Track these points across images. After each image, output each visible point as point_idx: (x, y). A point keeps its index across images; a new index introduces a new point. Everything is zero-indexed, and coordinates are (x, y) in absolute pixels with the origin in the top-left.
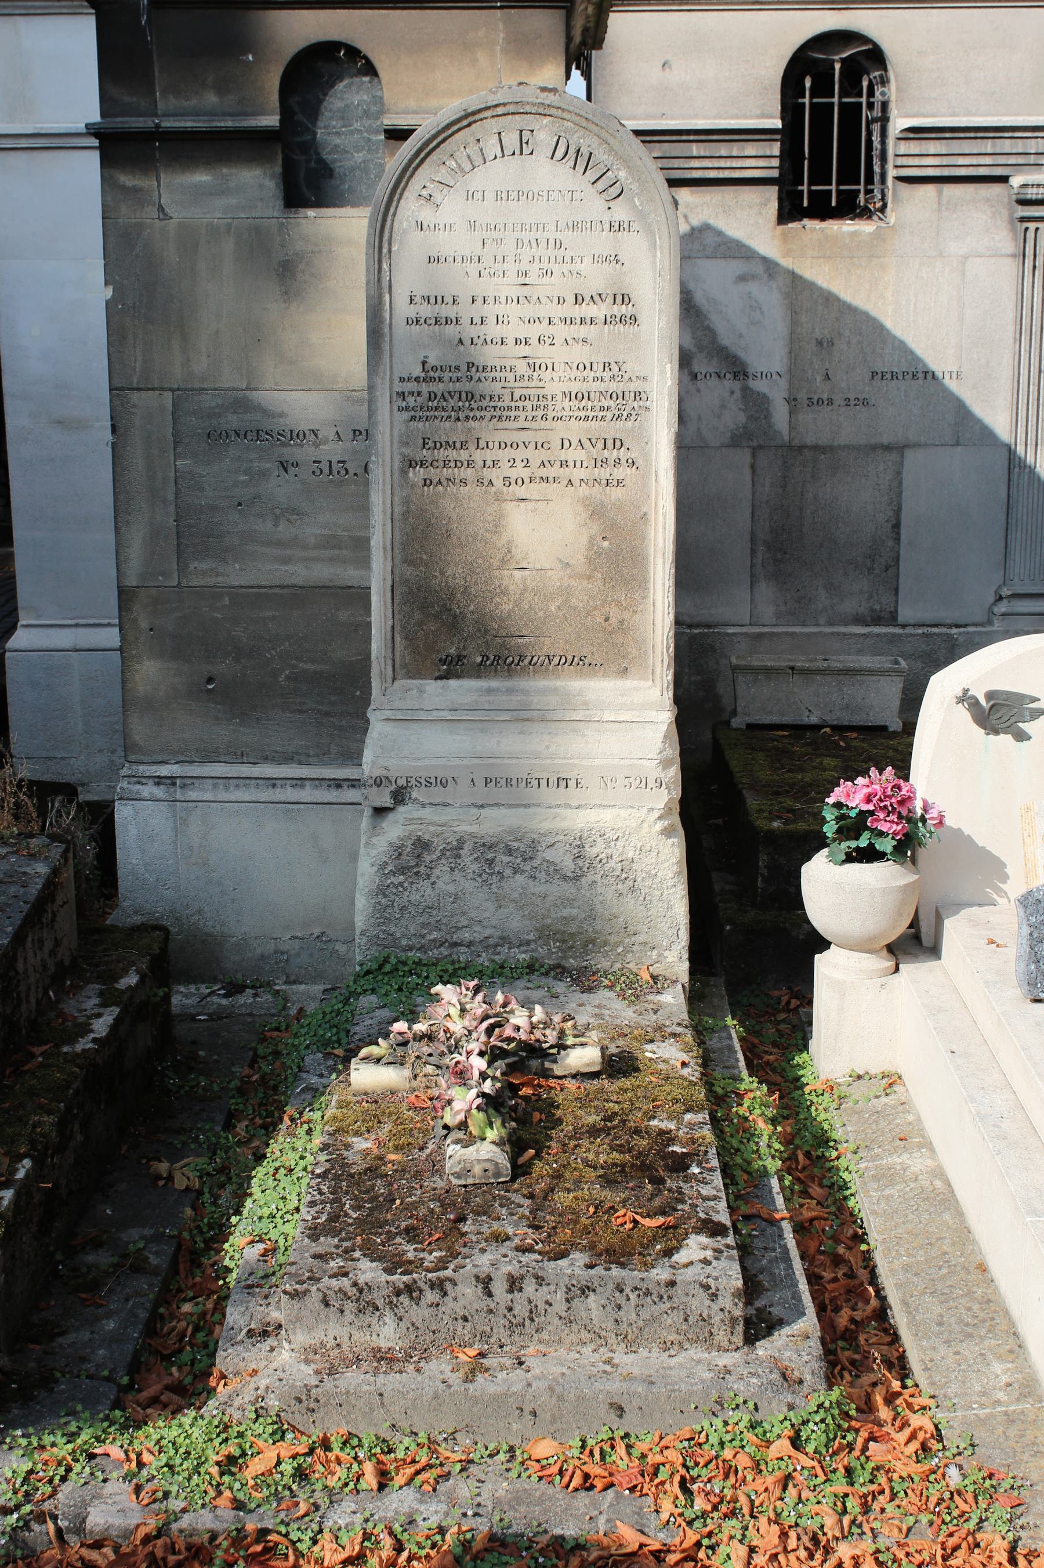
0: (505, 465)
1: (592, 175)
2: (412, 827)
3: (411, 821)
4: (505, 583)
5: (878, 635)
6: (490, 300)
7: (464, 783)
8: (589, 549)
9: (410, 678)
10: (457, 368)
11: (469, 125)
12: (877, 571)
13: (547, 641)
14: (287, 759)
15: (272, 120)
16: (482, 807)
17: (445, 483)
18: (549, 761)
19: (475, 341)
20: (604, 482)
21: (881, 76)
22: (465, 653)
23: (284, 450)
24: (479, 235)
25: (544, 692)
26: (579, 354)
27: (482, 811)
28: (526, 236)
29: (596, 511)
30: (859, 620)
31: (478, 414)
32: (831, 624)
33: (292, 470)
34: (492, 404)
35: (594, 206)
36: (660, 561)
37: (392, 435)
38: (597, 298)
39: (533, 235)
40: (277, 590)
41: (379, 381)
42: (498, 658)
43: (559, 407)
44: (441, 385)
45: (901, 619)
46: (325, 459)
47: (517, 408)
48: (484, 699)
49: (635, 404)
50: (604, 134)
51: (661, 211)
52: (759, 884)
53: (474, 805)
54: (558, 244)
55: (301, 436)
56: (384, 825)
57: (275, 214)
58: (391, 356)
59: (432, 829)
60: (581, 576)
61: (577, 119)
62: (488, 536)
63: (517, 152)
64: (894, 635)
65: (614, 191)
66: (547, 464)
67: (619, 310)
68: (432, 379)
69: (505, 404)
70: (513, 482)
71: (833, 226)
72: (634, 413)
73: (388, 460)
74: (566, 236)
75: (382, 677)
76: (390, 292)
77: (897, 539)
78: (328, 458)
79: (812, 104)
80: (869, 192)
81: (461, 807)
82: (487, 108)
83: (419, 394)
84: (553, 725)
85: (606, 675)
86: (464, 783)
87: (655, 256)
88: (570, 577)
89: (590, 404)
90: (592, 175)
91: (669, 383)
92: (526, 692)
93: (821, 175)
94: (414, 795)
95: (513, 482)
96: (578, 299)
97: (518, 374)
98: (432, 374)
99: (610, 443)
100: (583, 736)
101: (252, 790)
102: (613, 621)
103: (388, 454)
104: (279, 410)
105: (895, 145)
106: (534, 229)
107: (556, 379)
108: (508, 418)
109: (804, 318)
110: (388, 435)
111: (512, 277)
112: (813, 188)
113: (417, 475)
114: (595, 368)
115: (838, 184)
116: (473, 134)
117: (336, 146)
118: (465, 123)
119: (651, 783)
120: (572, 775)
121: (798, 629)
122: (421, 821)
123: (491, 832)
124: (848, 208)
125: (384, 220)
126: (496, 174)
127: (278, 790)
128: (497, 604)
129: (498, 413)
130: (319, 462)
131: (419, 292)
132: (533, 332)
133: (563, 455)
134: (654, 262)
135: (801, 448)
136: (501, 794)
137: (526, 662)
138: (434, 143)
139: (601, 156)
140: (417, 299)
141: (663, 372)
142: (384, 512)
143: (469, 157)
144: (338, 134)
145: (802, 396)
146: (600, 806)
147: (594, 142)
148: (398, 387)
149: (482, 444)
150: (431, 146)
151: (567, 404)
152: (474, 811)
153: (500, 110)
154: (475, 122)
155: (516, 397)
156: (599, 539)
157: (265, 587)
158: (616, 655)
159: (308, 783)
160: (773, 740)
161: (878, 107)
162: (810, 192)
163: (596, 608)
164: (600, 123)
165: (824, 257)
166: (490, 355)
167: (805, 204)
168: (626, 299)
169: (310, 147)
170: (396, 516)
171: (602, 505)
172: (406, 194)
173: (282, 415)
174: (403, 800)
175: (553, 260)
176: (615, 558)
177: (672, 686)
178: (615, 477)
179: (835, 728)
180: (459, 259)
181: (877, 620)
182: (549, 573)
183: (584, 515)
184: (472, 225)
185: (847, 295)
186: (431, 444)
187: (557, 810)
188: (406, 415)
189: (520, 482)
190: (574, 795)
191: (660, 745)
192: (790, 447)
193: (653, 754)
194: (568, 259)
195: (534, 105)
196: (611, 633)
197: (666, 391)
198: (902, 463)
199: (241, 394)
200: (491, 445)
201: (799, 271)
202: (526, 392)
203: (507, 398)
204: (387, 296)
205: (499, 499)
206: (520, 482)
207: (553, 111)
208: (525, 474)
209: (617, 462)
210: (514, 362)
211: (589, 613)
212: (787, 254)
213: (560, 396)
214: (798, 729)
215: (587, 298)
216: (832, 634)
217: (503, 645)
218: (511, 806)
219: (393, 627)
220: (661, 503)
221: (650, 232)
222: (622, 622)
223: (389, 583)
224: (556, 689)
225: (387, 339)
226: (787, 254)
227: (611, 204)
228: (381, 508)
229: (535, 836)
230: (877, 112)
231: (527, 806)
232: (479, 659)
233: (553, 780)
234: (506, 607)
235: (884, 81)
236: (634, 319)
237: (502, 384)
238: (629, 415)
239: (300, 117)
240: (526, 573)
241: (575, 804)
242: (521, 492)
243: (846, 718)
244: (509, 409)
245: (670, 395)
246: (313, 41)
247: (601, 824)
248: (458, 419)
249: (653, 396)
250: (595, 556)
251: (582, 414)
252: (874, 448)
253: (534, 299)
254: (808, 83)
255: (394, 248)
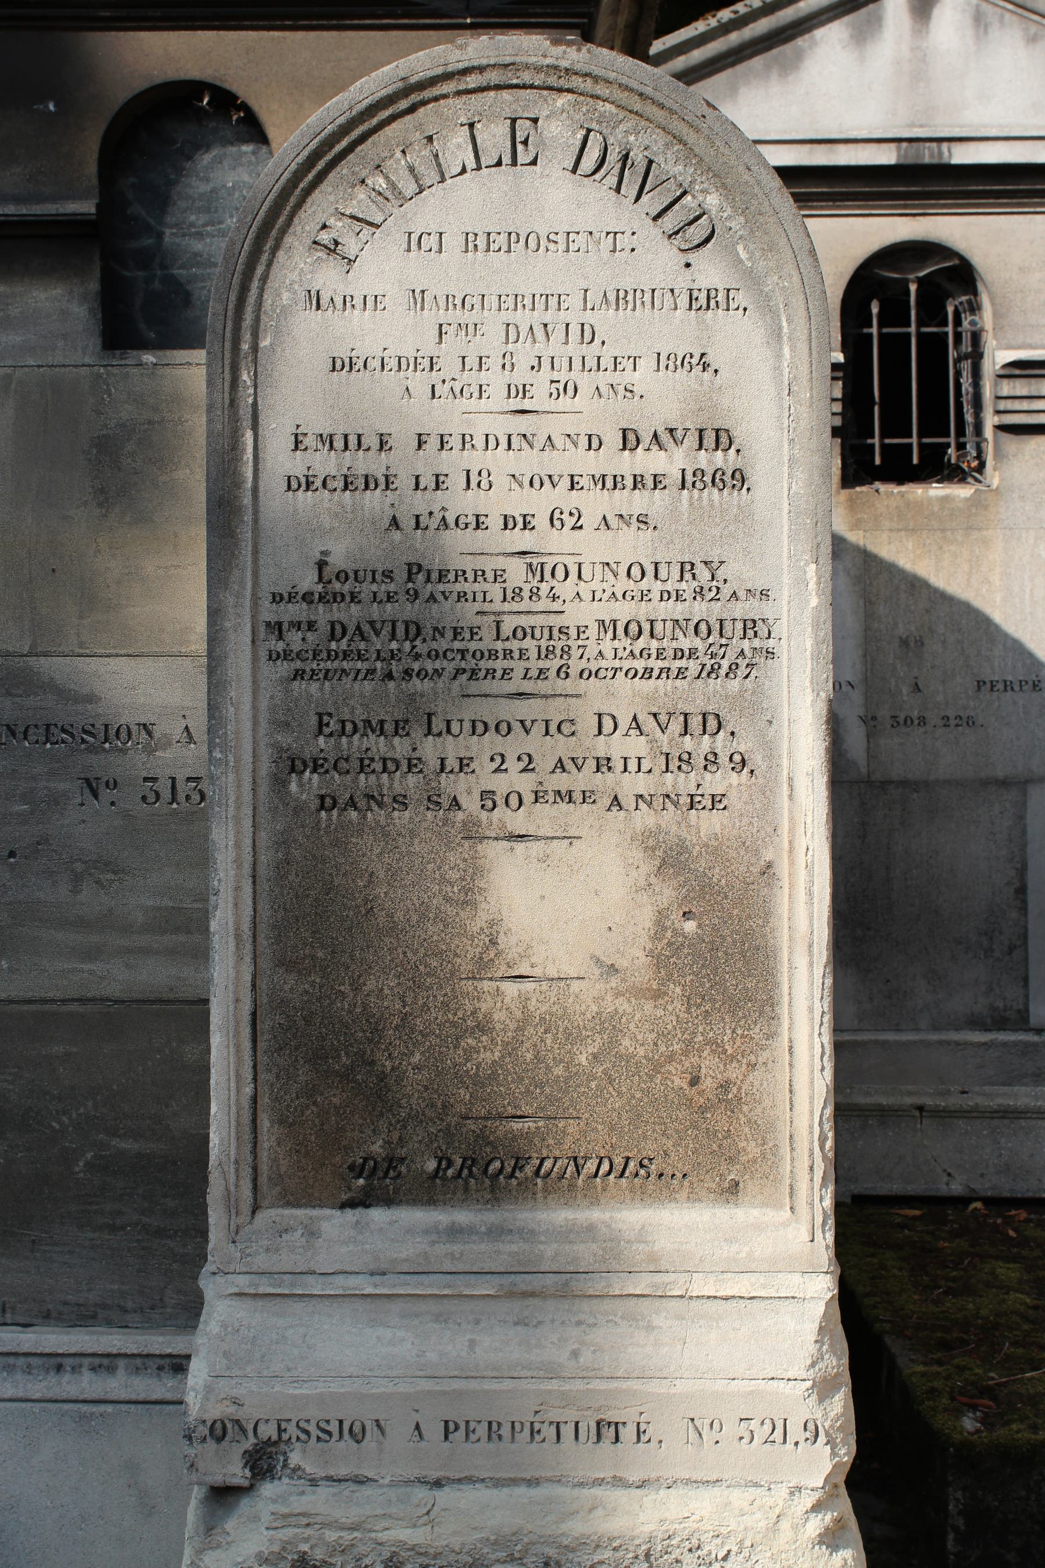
0: (484, 767)
1: (652, 202)
2: (287, 1533)
3: (286, 1519)
4: (484, 1007)
5: (1005, 1044)
6: (455, 442)
7: (400, 1432)
8: (656, 937)
9: (289, 1204)
10: (388, 575)
11: (412, 109)
12: (997, 954)
13: (573, 1127)
14: (84, 1316)
15: (87, 207)
16: (438, 1484)
17: (362, 803)
18: (579, 1385)
19: (424, 521)
20: (685, 800)
21: (969, 302)
22: (403, 1152)
23: (93, 759)
24: (431, 317)
25: (567, 1234)
26: (631, 546)
27: (438, 1493)
28: (523, 318)
29: (671, 859)
30: (975, 1023)
31: (429, 666)
32: (935, 1028)
33: (106, 794)
34: (457, 645)
35: (658, 262)
36: (801, 962)
37: (255, 708)
38: (665, 437)
39: (538, 317)
40: (74, 1007)
41: (231, 600)
42: (469, 1162)
43: (592, 650)
44: (354, 608)
45: (1033, 1021)
46: (164, 774)
47: (508, 654)
48: (441, 1249)
49: (746, 645)
50: (677, 126)
51: (790, 268)
52: (950, 1544)
53: (422, 1481)
54: (588, 335)
55: (124, 735)
56: (230, 1525)
57: (87, 360)
58: (256, 552)
59: (331, 1536)
60: (638, 993)
61: (622, 96)
62: (451, 911)
63: (507, 159)
64: (1027, 1044)
65: (696, 233)
66: (569, 765)
67: (709, 460)
68: (338, 597)
69: (483, 646)
70: (501, 801)
71: (917, 491)
72: (743, 663)
73: (247, 758)
74: (604, 320)
75: (231, 1204)
76: (255, 427)
77: (1024, 909)
78: (169, 772)
79: (881, 335)
80: (961, 446)
81: (392, 1484)
82: (447, 76)
83: (311, 626)
84: (586, 1305)
85: (694, 1198)
86: (400, 1432)
87: (779, 356)
88: (618, 994)
89: (654, 644)
90: (652, 202)
91: (814, 601)
92: (529, 1235)
93: (895, 424)
94: (295, 1458)
95: (501, 801)
96: (629, 440)
97: (510, 586)
98: (337, 586)
99: (695, 722)
100: (650, 1328)
101: (19, 1376)
102: (708, 1083)
103: (247, 747)
104: (86, 690)
105: (996, 385)
106: (540, 304)
107: (587, 596)
108: (491, 673)
109: (882, 610)
110: (247, 707)
111: (497, 399)
112: (887, 441)
113: (306, 787)
114: (663, 573)
115: (920, 436)
116: (419, 127)
117: (196, 254)
118: (404, 104)
119: (795, 1433)
120: (627, 1415)
121: (891, 1037)
122: (306, 1519)
123: (456, 1543)
124: (936, 468)
125: (244, 289)
126: (464, 203)
127: (67, 1377)
128: (470, 1051)
129: (470, 663)
130: (154, 780)
131: (316, 424)
132: (539, 503)
133: (601, 747)
134: (777, 368)
135: (885, 784)
136: (477, 1457)
137: (529, 1170)
138: (344, 143)
139: (671, 166)
140: (309, 441)
141: (801, 581)
142: (238, 862)
143: (412, 169)
144: (200, 236)
145: (884, 713)
146: (688, 1482)
147: (656, 140)
148: (269, 613)
149: (438, 725)
150: (338, 148)
151: (607, 646)
152: (421, 1493)
153: (472, 81)
154: (424, 103)
155: (507, 629)
156: (676, 916)
157: (53, 1001)
158: (714, 1156)
159: (121, 1363)
160: (902, 1226)
161: (967, 339)
162: (883, 446)
163: (671, 1058)
164: (669, 103)
165: (906, 530)
166: (457, 548)
167: (878, 461)
168: (724, 439)
169: (154, 258)
170: (262, 871)
171: (682, 847)
172: (288, 240)
173: (91, 698)
174: (271, 1469)
175: (577, 364)
176: (711, 957)
177: (831, 1222)
178: (708, 789)
179: (988, 1201)
180: (392, 363)
181: (1000, 1022)
182: (575, 986)
183: (645, 869)
184: (418, 298)
185: (939, 581)
186: (334, 726)
187: (597, 1491)
188: (284, 668)
189: (514, 801)
190: (635, 1463)
191: (812, 1348)
192: (869, 783)
193: (798, 1370)
194: (607, 362)
195: (538, 69)
196: (703, 1110)
197: (807, 617)
198: (1024, 805)
199: (20, 662)
200: (455, 728)
201: (872, 548)
202: (524, 621)
203: (487, 634)
204: (249, 435)
205: (473, 834)
206: (514, 801)
207: (576, 82)
208: (525, 784)
209: (711, 761)
210: (501, 563)
211: (657, 1067)
212: (856, 525)
213: (593, 631)
214: (935, 1204)
215: (646, 438)
216: (941, 1043)
217: (481, 1136)
218: (498, 1483)
219: (254, 1099)
220: (802, 843)
221: (767, 308)
222: (725, 1086)
223: (247, 1007)
224: (591, 1229)
225: (248, 518)
226: (856, 525)
227: (691, 257)
228: (231, 854)
229: (552, 1552)
230: (966, 347)
231: (533, 1482)
232: (431, 1165)
233: (588, 1425)
234: (486, 1057)
235: (974, 308)
236: (740, 478)
237: (477, 606)
238: (733, 667)
239: (137, 209)
240: (528, 986)
241: (634, 1477)
242: (517, 821)
243: (1006, 1187)
244: (493, 654)
245: (816, 626)
246: (158, 81)
247: (691, 1525)
248: (389, 676)
249: (781, 629)
250: (669, 954)
251: (640, 664)
252: (986, 783)
253: (540, 440)
254: (875, 309)
255: (265, 343)
